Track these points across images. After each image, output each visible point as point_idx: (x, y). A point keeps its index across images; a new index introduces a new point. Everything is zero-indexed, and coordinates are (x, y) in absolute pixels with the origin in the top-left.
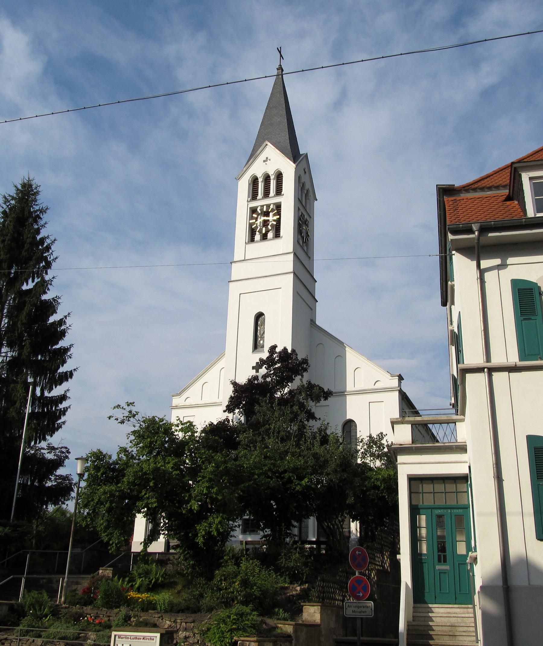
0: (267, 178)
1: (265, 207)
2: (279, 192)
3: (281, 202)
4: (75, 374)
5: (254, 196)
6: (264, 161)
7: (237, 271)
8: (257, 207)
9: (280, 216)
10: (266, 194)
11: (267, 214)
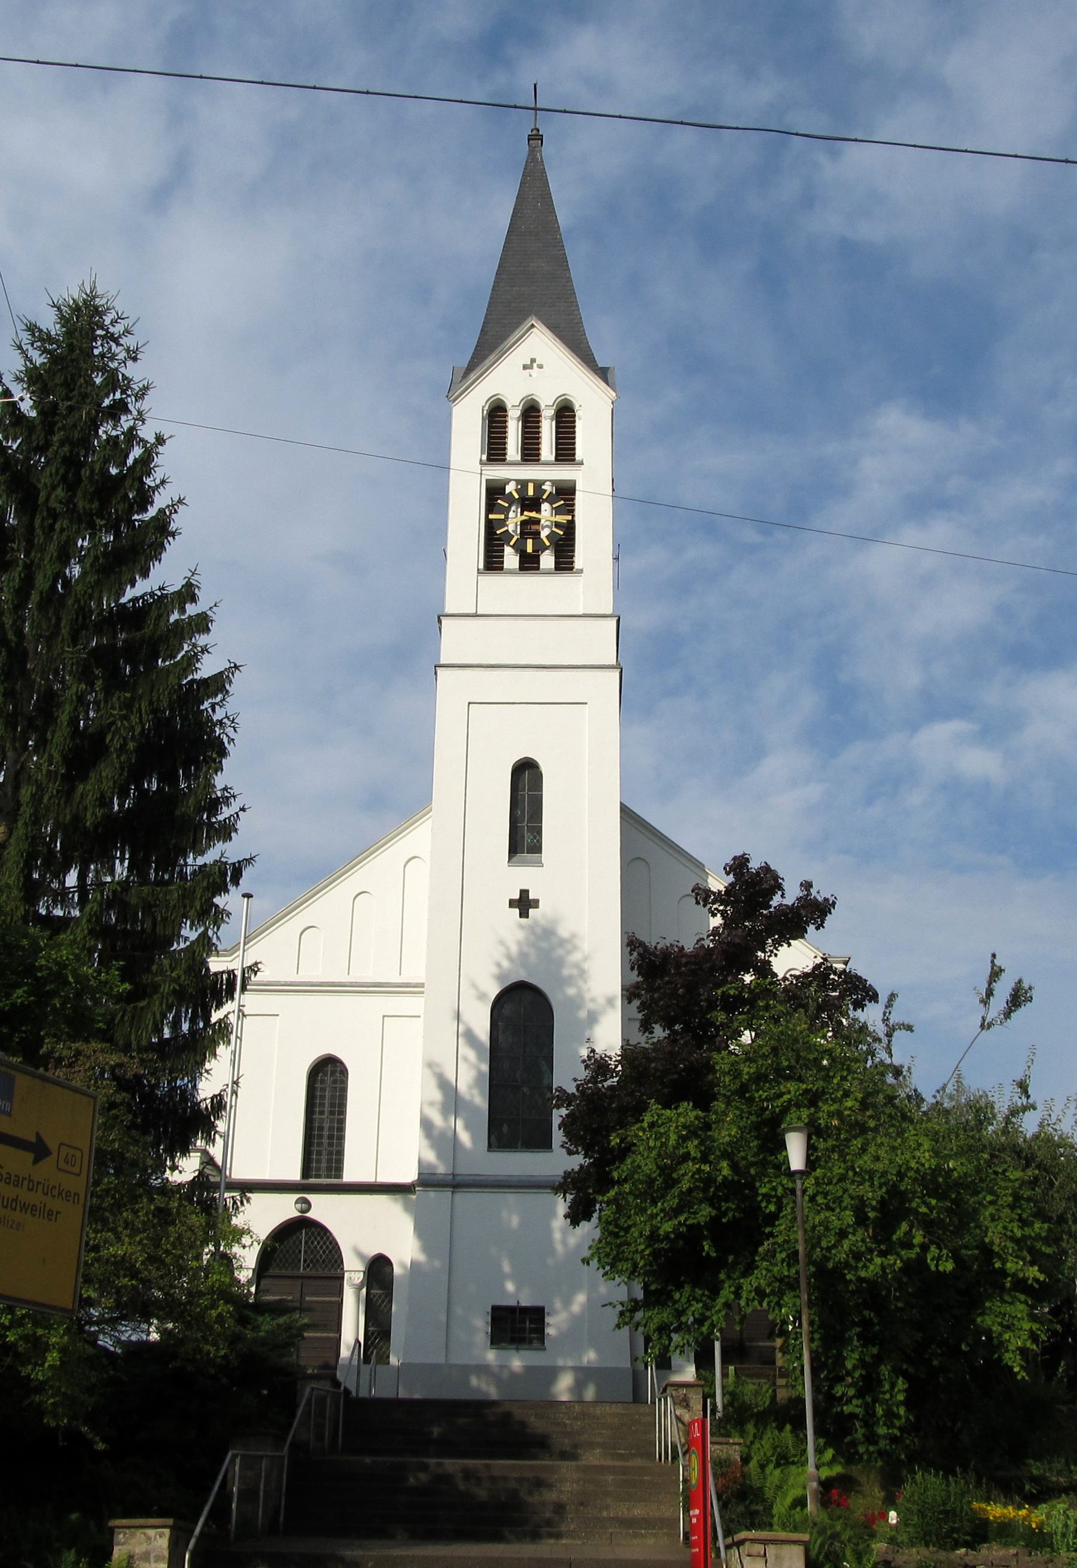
0: (531, 413)
1: (531, 486)
2: (565, 452)
3: (575, 482)
4: (247, 873)
5: (495, 451)
6: (525, 367)
7: (456, 641)
8: (508, 481)
9: (573, 516)
10: (530, 453)
11: (531, 504)
